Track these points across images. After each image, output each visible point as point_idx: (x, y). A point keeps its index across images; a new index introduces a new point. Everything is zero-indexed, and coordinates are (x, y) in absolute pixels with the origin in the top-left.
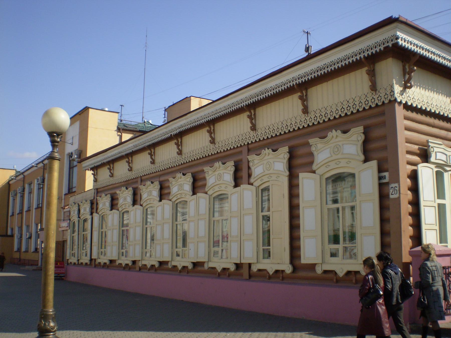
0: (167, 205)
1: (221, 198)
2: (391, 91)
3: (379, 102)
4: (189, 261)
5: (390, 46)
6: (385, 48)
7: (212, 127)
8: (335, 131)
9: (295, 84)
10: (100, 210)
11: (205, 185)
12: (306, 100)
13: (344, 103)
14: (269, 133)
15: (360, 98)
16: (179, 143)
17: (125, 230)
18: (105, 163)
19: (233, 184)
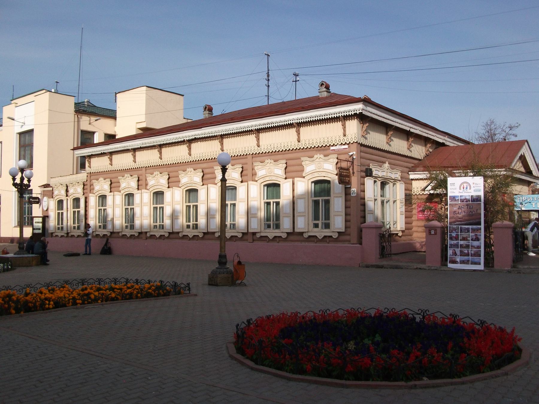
8: (319, 155)
9: (294, 122)
10: (96, 191)
11: (119, 187)
13: (325, 139)
19: (109, 191)
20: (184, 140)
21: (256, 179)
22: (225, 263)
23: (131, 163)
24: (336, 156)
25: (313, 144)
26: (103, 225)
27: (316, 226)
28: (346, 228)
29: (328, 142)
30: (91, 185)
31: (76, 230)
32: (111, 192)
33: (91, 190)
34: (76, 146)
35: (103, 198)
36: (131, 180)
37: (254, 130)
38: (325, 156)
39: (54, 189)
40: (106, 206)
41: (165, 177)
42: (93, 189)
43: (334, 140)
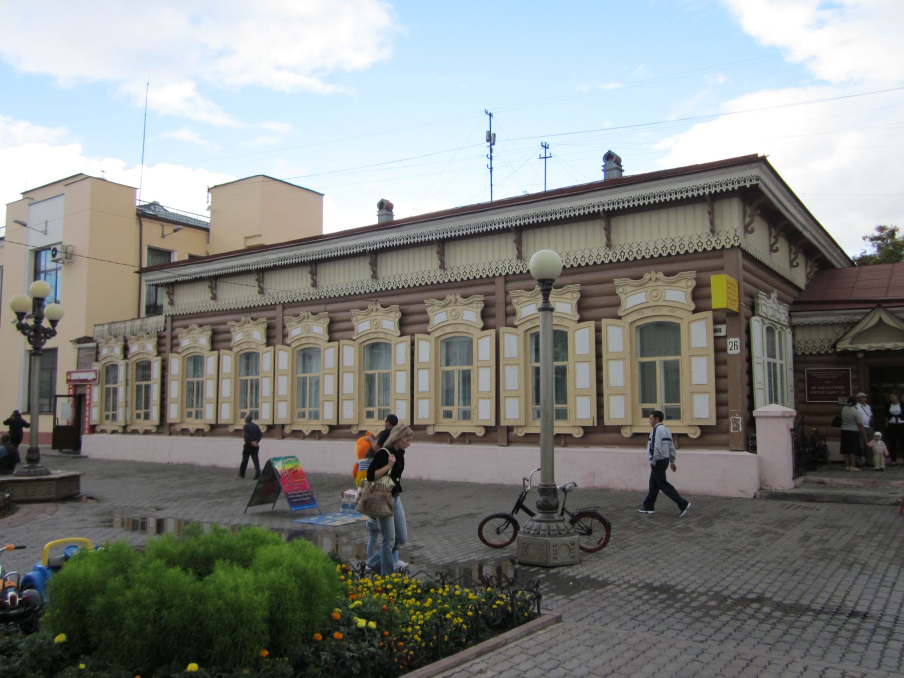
4: (324, 423)
5: (748, 186)
6: (739, 188)
7: (171, 289)
10: (360, 335)
11: (230, 340)
12: (263, 281)
16: (214, 286)
17: (454, 371)
20: (364, 251)
21: (516, 323)
22: (37, 460)
23: (254, 296)
24: (482, 298)
25: (639, 252)
26: (379, 410)
27: (448, 415)
28: (719, 417)
29: (400, 282)
30: (174, 338)
33: (174, 346)
34: (145, 265)
35: (196, 362)
37: (512, 229)
38: (667, 274)
39: (100, 345)
41: (570, 298)
42: (178, 345)
43: (686, 243)
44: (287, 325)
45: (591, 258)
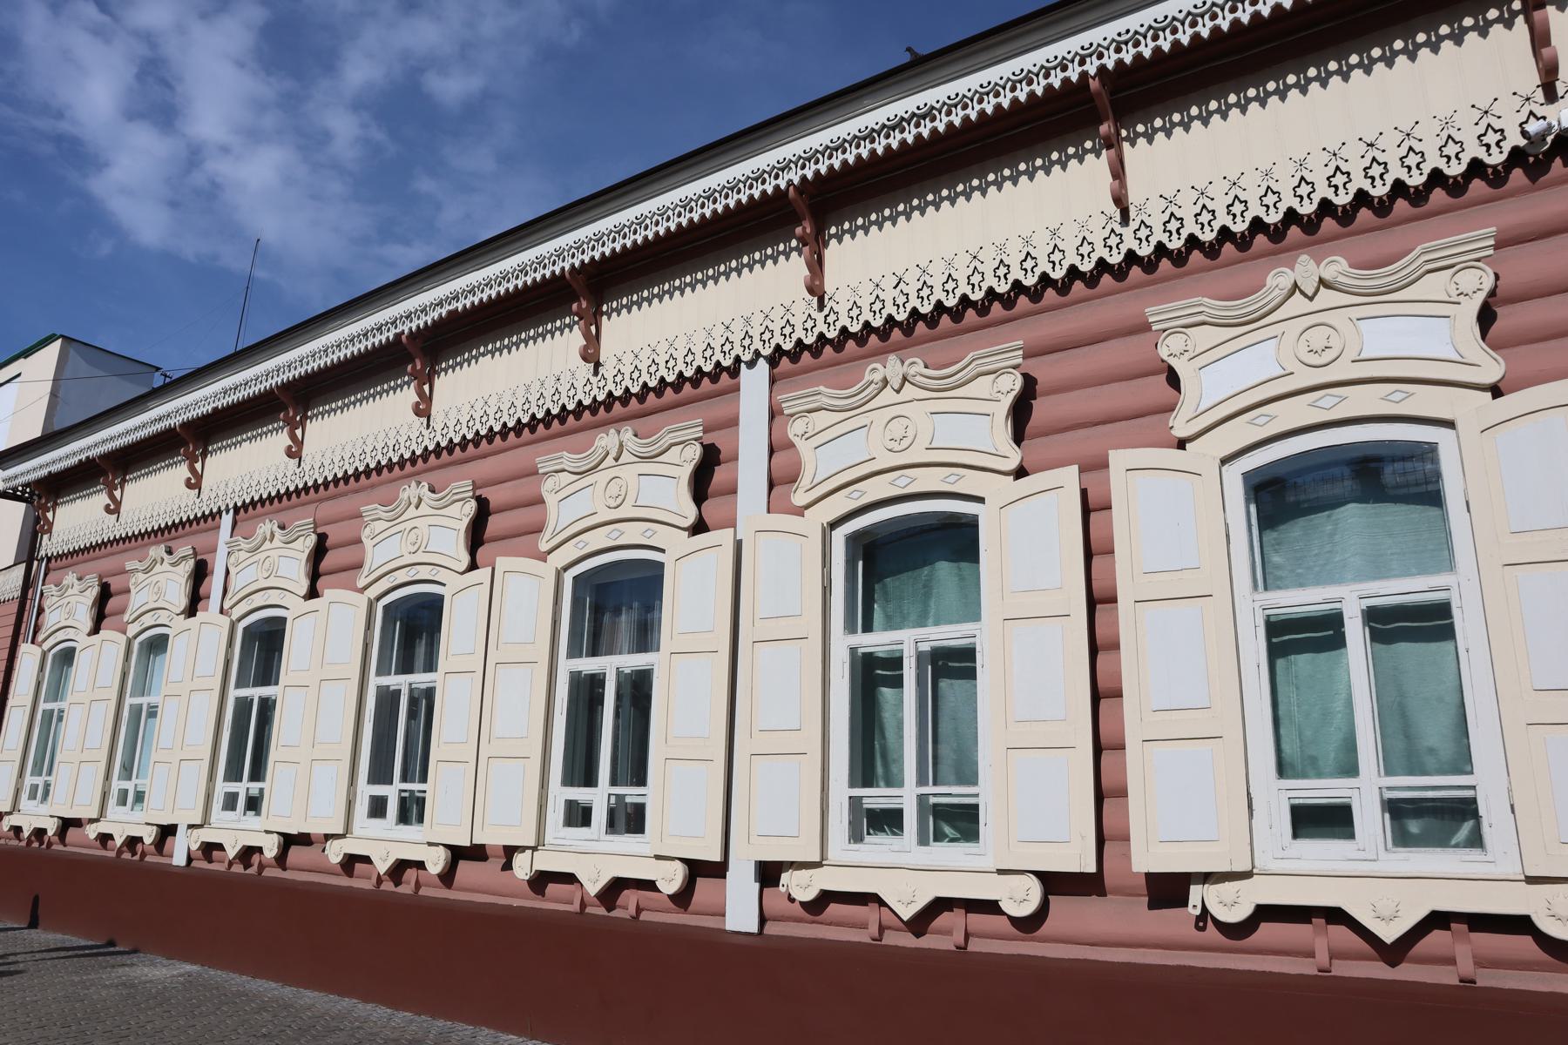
0: (111, 643)
1: (157, 645)
2: (974, 272)
3: (1235, 223)
14: (902, 299)
15: (747, 321)
18: (94, 459)
27: (579, 815)
31: (388, 825)
32: (473, 566)
36: (431, 520)
40: (430, 667)
44: (795, 429)
45: (976, 279)
